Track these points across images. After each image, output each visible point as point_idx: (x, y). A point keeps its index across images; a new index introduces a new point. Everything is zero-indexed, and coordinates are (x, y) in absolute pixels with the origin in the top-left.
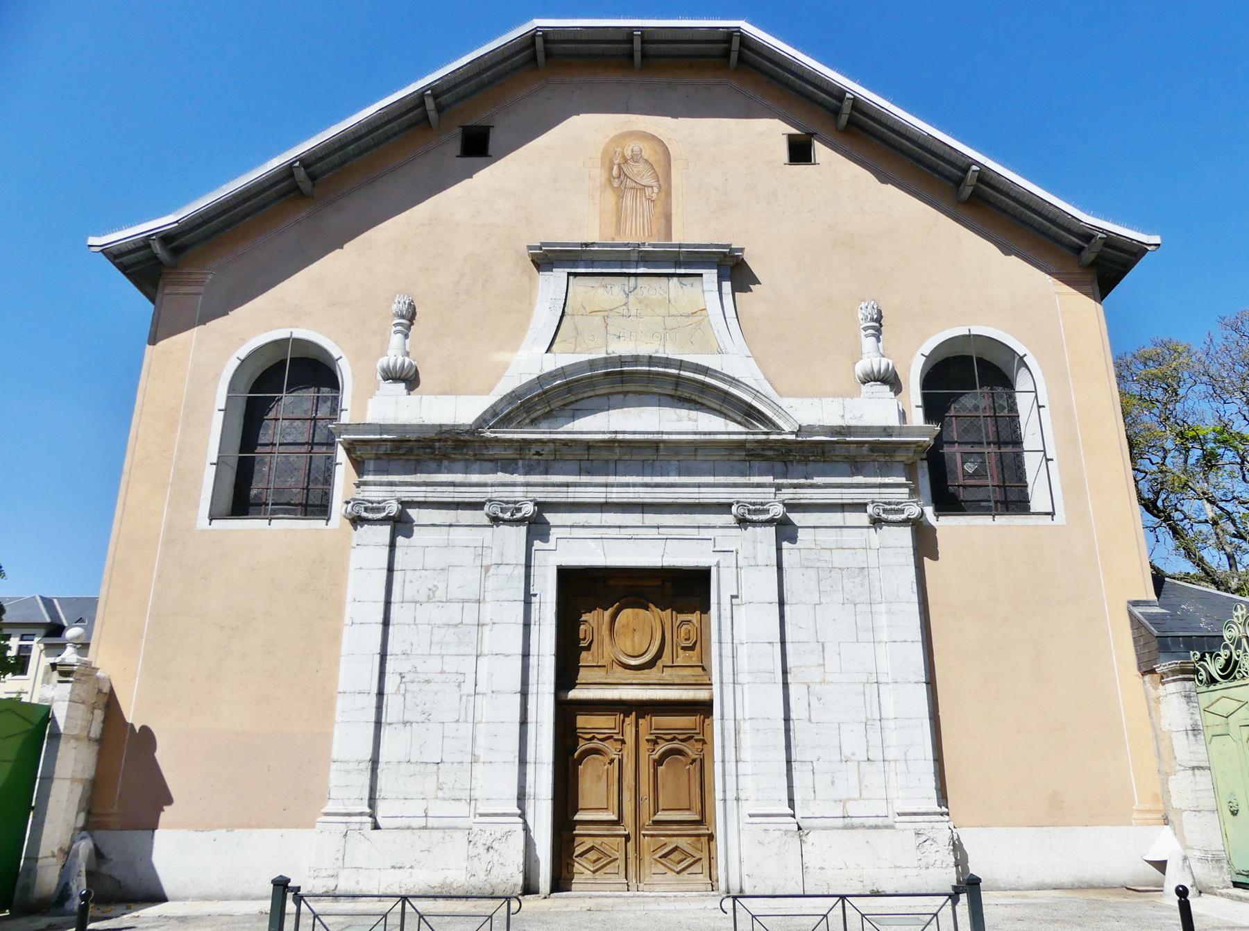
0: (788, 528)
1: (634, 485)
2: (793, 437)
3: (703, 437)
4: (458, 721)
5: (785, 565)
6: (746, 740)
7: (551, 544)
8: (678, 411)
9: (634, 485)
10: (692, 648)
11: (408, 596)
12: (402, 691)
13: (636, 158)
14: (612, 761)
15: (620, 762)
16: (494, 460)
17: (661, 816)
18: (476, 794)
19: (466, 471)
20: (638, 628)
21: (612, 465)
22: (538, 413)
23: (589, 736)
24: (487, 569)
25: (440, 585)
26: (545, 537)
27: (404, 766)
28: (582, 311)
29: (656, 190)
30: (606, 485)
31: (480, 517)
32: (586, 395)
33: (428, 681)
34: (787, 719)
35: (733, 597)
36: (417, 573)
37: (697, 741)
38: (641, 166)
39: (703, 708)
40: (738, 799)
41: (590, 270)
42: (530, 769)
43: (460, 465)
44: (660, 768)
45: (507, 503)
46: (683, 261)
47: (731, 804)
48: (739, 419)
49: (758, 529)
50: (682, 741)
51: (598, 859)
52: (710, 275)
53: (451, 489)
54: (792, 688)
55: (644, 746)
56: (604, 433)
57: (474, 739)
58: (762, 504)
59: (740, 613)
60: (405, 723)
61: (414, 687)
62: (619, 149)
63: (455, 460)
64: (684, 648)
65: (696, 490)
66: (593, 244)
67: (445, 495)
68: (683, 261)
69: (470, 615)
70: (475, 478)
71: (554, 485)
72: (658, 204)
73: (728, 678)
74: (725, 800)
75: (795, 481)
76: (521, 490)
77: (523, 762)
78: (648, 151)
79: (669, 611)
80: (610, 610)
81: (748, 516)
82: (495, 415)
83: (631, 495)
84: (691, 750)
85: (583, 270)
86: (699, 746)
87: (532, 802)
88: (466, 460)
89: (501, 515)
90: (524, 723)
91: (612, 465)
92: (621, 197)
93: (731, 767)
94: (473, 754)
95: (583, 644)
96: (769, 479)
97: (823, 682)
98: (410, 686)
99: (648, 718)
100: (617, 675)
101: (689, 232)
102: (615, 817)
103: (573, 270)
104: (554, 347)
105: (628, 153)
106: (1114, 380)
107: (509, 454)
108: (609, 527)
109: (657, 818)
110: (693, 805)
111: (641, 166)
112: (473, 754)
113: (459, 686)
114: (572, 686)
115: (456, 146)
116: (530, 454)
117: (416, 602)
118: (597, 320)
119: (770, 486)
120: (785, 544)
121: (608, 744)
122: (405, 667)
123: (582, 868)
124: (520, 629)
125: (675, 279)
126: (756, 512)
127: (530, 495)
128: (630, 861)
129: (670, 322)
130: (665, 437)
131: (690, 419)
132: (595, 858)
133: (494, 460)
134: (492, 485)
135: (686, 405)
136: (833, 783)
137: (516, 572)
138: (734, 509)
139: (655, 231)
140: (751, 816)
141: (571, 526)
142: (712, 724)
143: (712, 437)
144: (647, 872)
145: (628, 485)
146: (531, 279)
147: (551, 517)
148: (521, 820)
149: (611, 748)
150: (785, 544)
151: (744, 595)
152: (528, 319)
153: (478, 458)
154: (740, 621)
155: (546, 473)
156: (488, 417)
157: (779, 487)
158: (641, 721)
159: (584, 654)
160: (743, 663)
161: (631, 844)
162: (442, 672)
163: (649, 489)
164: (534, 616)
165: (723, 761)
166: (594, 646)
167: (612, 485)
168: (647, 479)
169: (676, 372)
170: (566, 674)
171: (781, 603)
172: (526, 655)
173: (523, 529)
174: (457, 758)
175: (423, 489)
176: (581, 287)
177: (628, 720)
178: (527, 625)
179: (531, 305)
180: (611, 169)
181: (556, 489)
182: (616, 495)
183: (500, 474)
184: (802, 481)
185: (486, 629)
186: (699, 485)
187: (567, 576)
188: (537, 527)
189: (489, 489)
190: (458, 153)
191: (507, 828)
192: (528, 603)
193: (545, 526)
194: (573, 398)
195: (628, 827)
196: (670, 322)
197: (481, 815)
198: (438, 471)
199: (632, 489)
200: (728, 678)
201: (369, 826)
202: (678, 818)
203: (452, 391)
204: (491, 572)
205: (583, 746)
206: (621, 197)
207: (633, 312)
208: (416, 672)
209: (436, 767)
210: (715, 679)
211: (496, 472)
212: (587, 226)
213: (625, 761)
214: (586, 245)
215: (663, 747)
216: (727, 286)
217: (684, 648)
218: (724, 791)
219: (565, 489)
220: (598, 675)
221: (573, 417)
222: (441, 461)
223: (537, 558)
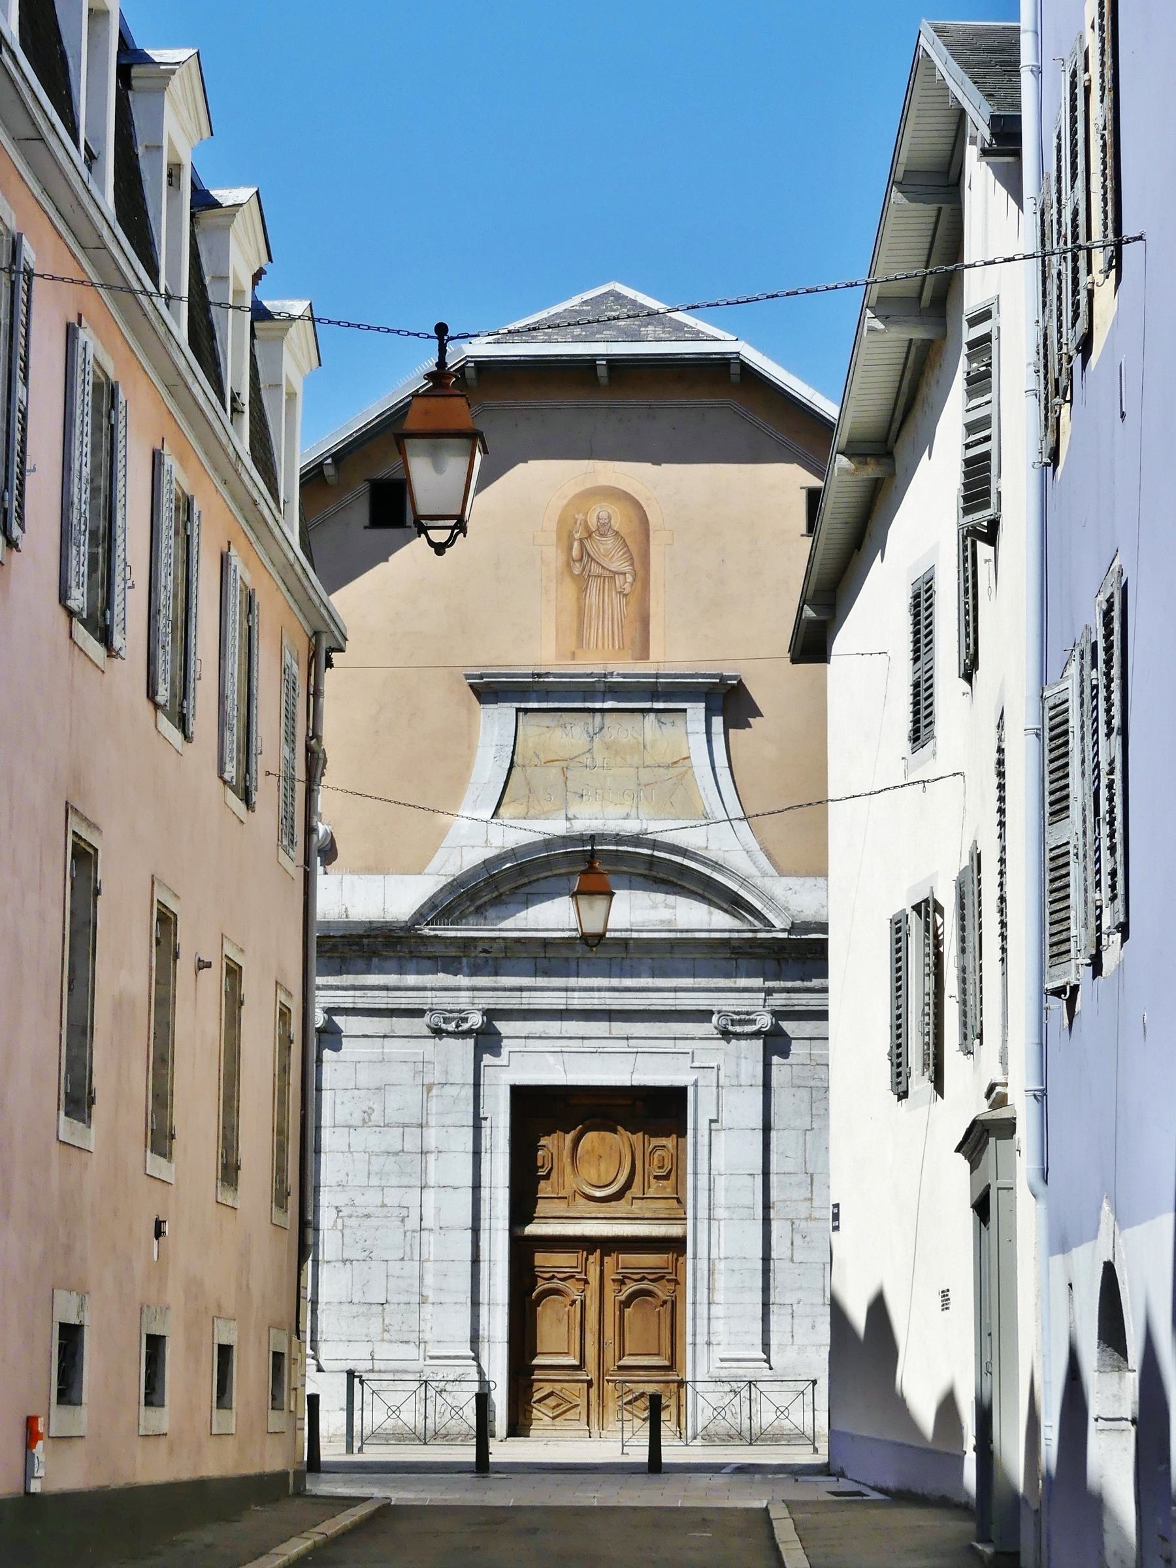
0: (780, 1040)
1: (599, 990)
2: (784, 935)
3: (679, 935)
4: (403, 1259)
5: (774, 1083)
6: (720, 1281)
7: (503, 1059)
8: (653, 895)
9: (599, 990)
10: (666, 1177)
11: (340, 1119)
12: (340, 1227)
13: (604, 529)
14: (574, 1302)
15: (583, 1304)
16: (433, 958)
17: (627, 1361)
18: (427, 1336)
19: (401, 971)
20: (604, 1153)
21: (573, 965)
22: (486, 899)
23: (547, 1275)
24: (429, 1088)
25: (375, 1107)
26: (496, 1051)
27: (345, 1307)
28: (536, 761)
29: (629, 578)
30: (566, 990)
31: (419, 1025)
32: (542, 875)
33: (368, 1216)
34: (766, 1259)
35: (711, 1121)
36: (349, 1093)
37: (668, 1281)
38: (609, 542)
39: (676, 1245)
40: (709, 1344)
41: (544, 705)
42: (483, 1310)
43: (392, 964)
44: (627, 1311)
45: (451, 1011)
46: (662, 694)
47: (702, 1349)
48: (725, 906)
49: (743, 1042)
50: (651, 1280)
51: (558, 1405)
52: (696, 711)
53: (384, 993)
54: (775, 1226)
55: (610, 1287)
56: (563, 930)
57: (421, 1278)
58: (748, 1013)
59: (720, 1140)
60: (344, 1261)
61: (353, 1222)
62: (580, 517)
63: (386, 958)
64: (656, 1177)
65: (672, 995)
66: (547, 675)
67: (377, 1000)
68: (662, 694)
69: (412, 1143)
70: (411, 980)
71: (505, 989)
72: (633, 599)
73: (703, 1213)
74: (695, 1344)
75: (789, 984)
76: (465, 994)
77: (475, 1303)
78: (619, 518)
79: (640, 1134)
80: (572, 1134)
81: (730, 1028)
82: (435, 907)
83: (596, 1001)
84: (658, 1289)
85: (535, 705)
86: (671, 1286)
87: (486, 1344)
88: (400, 958)
89: (444, 1026)
90: (476, 1261)
91: (573, 965)
92: (583, 590)
93: (702, 1309)
94: (421, 1295)
95: (542, 1172)
96: (758, 982)
97: (810, 1218)
98: (348, 1222)
99: (614, 1255)
100: (580, 1208)
101: (674, 653)
102: (576, 1362)
103: (523, 705)
104: (502, 810)
105: (593, 523)
106: (831, 1089)
107: (453, 952)
108: (571, 1038)
109: (622, 1363)
110: (663, 1350)
111: (609, 542)
112: (421, 1295)
113: (403, 1221)
114: (530, 1220)
115: (361, 512)
116: (477, 952)
117: (349, 1127)
118: (554, 772)
119: (759, 990)
120: (775, 1059)
121: (568, 1283)
122: (341, 1199)
123: (540, 1415)
124: (469, 1158)
125: (652, 716)
126: (741, 1022)
127: (476, 1001)
128: (592, 1408)
129: (646, 775)
130: (635, 935)
131: (667, 906)
132: (554, 1404)
133: (433, 958)
134: (432, 989)
135: (663, 887)
136: (813, 1327)
137: (463, 1093)
138: (715, 1018)
139: (627, 642)
140: (722, 1360)
141: (526, 1038)
142: (684, 1263)
143: (690, 935)
144: (611, 1419)
145: (592, 989)
146: (470, 711)
147: (503, 1027)
148: (475, 1363)
149: (573, 1289)
150: (775, 1059)
151: (725, 1117)
152: (468, 766)
153: (413, 956)
154: (721, 1149)
155: (496, 974)
156: (425, 911)
157: (769, 992)
158: (606, 1259)
159: (542, 1184)
160: (720, 1197)
161: (594, 1391)
162: (384, 1206)
163: (617, 994)
164: (485, 1143)
165: (694, 1303)
166: (554, 1175)
167: (573, 990)
168: (615, 982)
169: (649, 852)
170: (523, 1206)
171: (767, 1128)
172: (476, 1187)
173: (470, 1042)
174: (404, 1298)
175: (351, 993)
176: (533, 728)
177: (591, 1258)
178: (477, 1154)
179: (471, 748)
180: (570, 548)
181: (508, 994)
182: (578, 1001)
183: (441, 975)
184: (798, 984)
185: (431, 1158)
186: (675, 990)
187: (519, 1094)
188: (486, 1040)
189: (429, 994)
190: (367, 523)
191: (459, 1370)
192: (477, 1128)
193: (495, 1038)
194: (526, 880)
195: (591, 1372)
196: (646, 775)
197: (432, 1358)
198: (368, 971)
199: (596, 994)
200: (703, 1213)
201: (315, 1368)
202: (646, 1363)
203: (376, 867)
204: (434, 1092)
205: (542, 1286)
206: (583, 590)
207: (599, 762)
208: (353, 1205)
209: (381, 1308)
210: (690, 1214)
211: (435, 972)
212: (540, 652)
213: (588, 1301)
214: (539, 675)
215: (630, 1287)
216: (718, 722)
217: (656, 1177)
218: (694, 1335)
219: (518, 994)
220: (559, 1208)
221: (527, 903)
222: (369, 959)
223: (487, 1075)
